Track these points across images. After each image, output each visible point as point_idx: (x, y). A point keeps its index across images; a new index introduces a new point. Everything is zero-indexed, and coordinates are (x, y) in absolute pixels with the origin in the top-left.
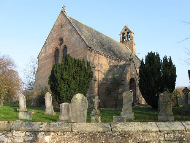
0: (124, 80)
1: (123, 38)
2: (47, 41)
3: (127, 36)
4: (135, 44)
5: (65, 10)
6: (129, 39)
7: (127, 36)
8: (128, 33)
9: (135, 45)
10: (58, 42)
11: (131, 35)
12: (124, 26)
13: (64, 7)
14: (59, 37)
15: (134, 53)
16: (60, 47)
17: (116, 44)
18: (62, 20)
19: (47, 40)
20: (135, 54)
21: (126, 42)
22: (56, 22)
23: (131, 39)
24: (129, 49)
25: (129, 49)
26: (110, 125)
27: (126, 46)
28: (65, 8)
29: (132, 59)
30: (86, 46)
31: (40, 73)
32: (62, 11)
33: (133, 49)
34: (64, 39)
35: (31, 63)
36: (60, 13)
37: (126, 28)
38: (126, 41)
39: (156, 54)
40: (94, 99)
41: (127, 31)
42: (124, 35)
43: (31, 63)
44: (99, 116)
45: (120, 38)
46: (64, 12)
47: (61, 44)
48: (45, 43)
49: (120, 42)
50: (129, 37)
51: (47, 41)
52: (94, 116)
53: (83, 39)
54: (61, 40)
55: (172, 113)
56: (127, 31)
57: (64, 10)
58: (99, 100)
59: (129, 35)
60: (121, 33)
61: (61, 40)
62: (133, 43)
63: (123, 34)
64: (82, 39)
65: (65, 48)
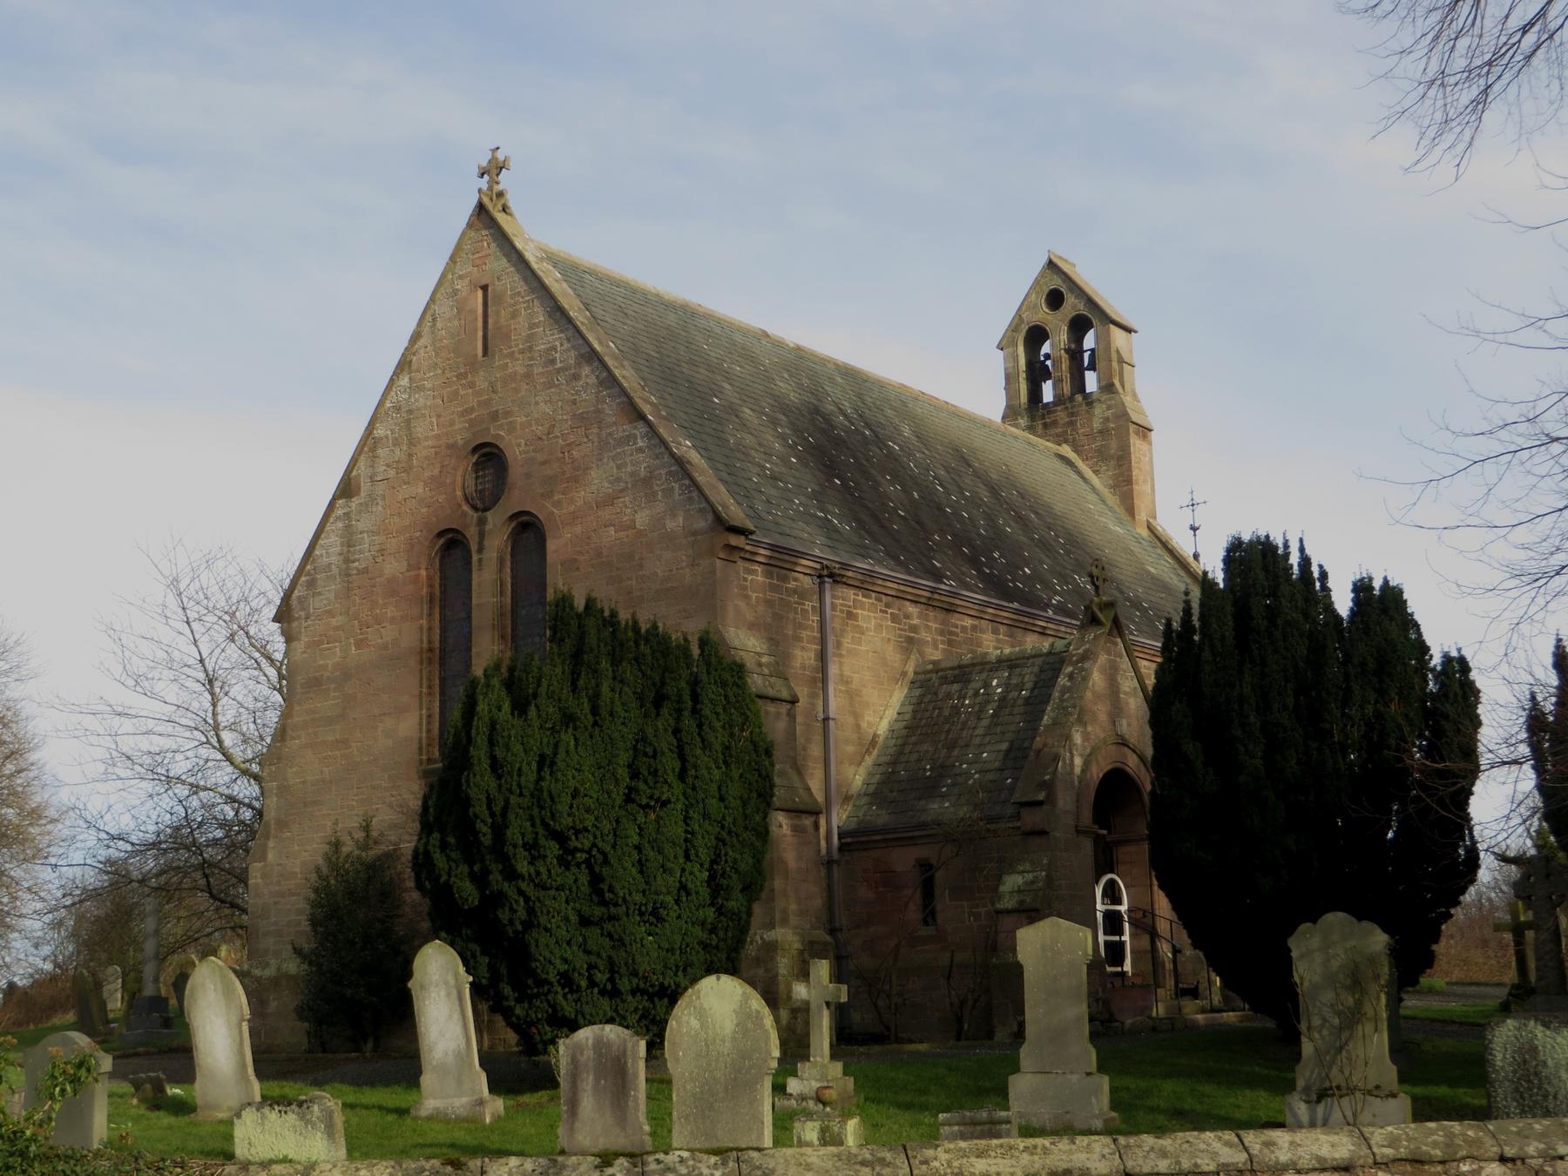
0: (1041, 796)
1: (1037, 372)
2: (362, 468)
3: (1075, 354)
4: (1144, 431)
5: (512, 200)
6: (1091, 381)
7: (1075, 354)
8: (1079, 326)
9: (1154, 436)
10: (461, 476)
11: (1104, 339)
12: (1044, 261)
13: (493, 169)
14: (461, 434)
15: (1142, 516)
16: (482, 522)
17: (962, 459)
18: (485, 288)
19: (354, 461)
20: (1150, 528)
21: (1061, 416)
22: (432, 299)
23: (1108, 388)
24: (1088, 473)
25: (1088, 473)
26: (903, 1156)
27: (1066, 450)
28: (505, 180)
29: (1110, 605)
30: (710, 517)
31: (1402, 1150)
32: (481, 208)
33: (1129, 481)
34: (516, 450)
35: (684, 899)
36: (470, 225)
37: (1056, 282)
38: (1059, 400)
39: (1294, 559)
40: (456, 443)
41: (1072, 306)
42: (1046, 348)
43: (684, 899)
44: (846, 1116)
45: (1010, 379)
46: (500, 217)
47: (483, 502)
48: (346, 489)
49: (1010, 414)
50: (1092, 367)
51: (362, 468)
52: (809, 1115)
53: (680, 462)
54: (489, 458)
55: (1390, 1073)
56: (1072, 306)
57: (500, 195)
58: (844, 988)
59: (1089, 341)
60: (1014, 328)
61: (489, 458)
62: (1123, 416)
63: (1036, 336)
64: (672, 455)
65: (528, 530)
